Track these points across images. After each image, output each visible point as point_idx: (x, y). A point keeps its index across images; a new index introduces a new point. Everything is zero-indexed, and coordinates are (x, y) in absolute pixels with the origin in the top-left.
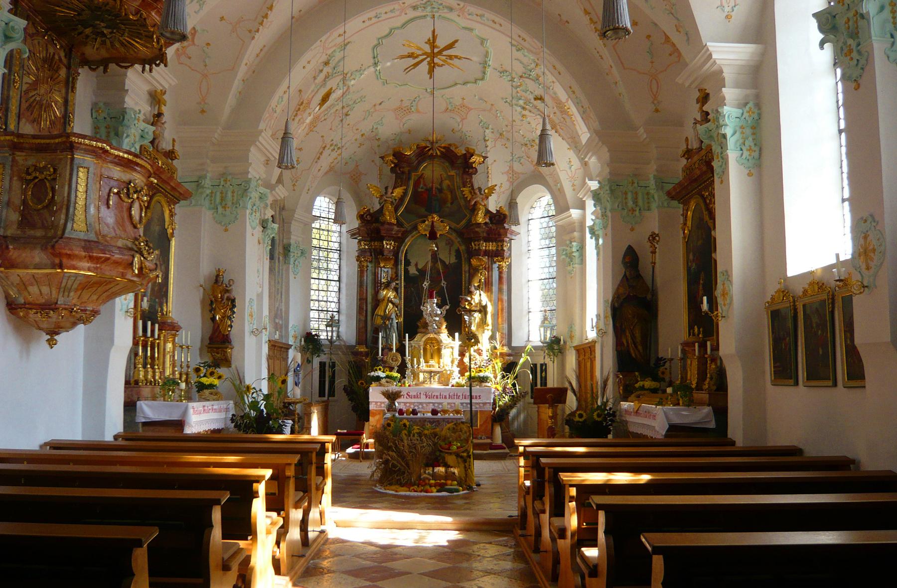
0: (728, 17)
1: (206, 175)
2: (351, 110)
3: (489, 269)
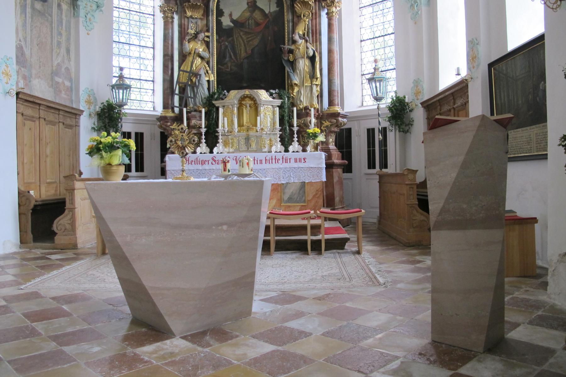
3: (316, 17)
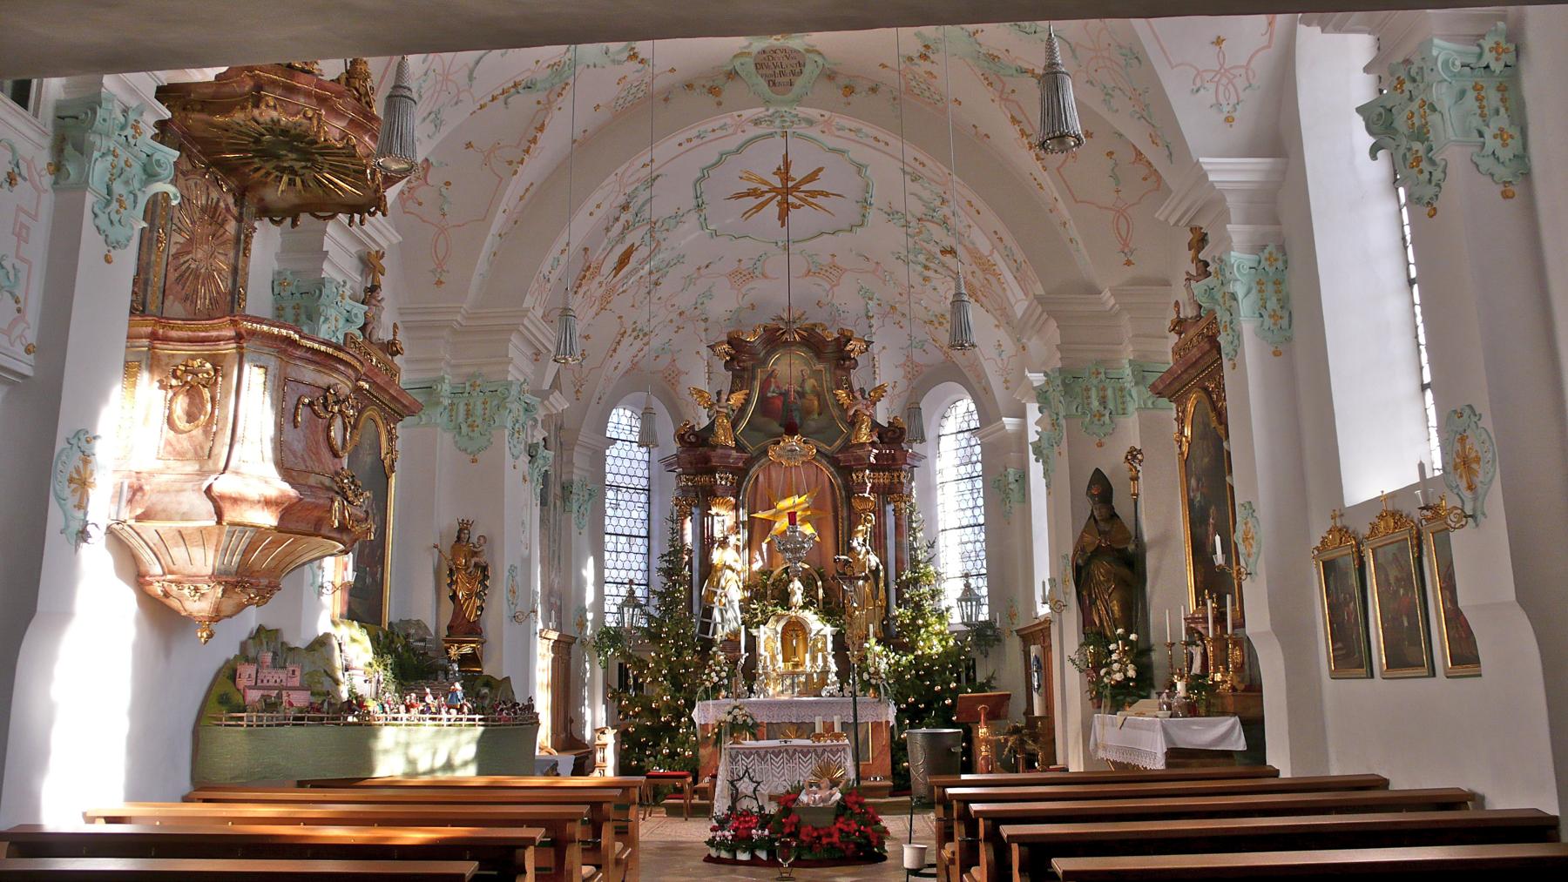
0: (1229, 120)
1: (443, 379)
2: (664, 276)
